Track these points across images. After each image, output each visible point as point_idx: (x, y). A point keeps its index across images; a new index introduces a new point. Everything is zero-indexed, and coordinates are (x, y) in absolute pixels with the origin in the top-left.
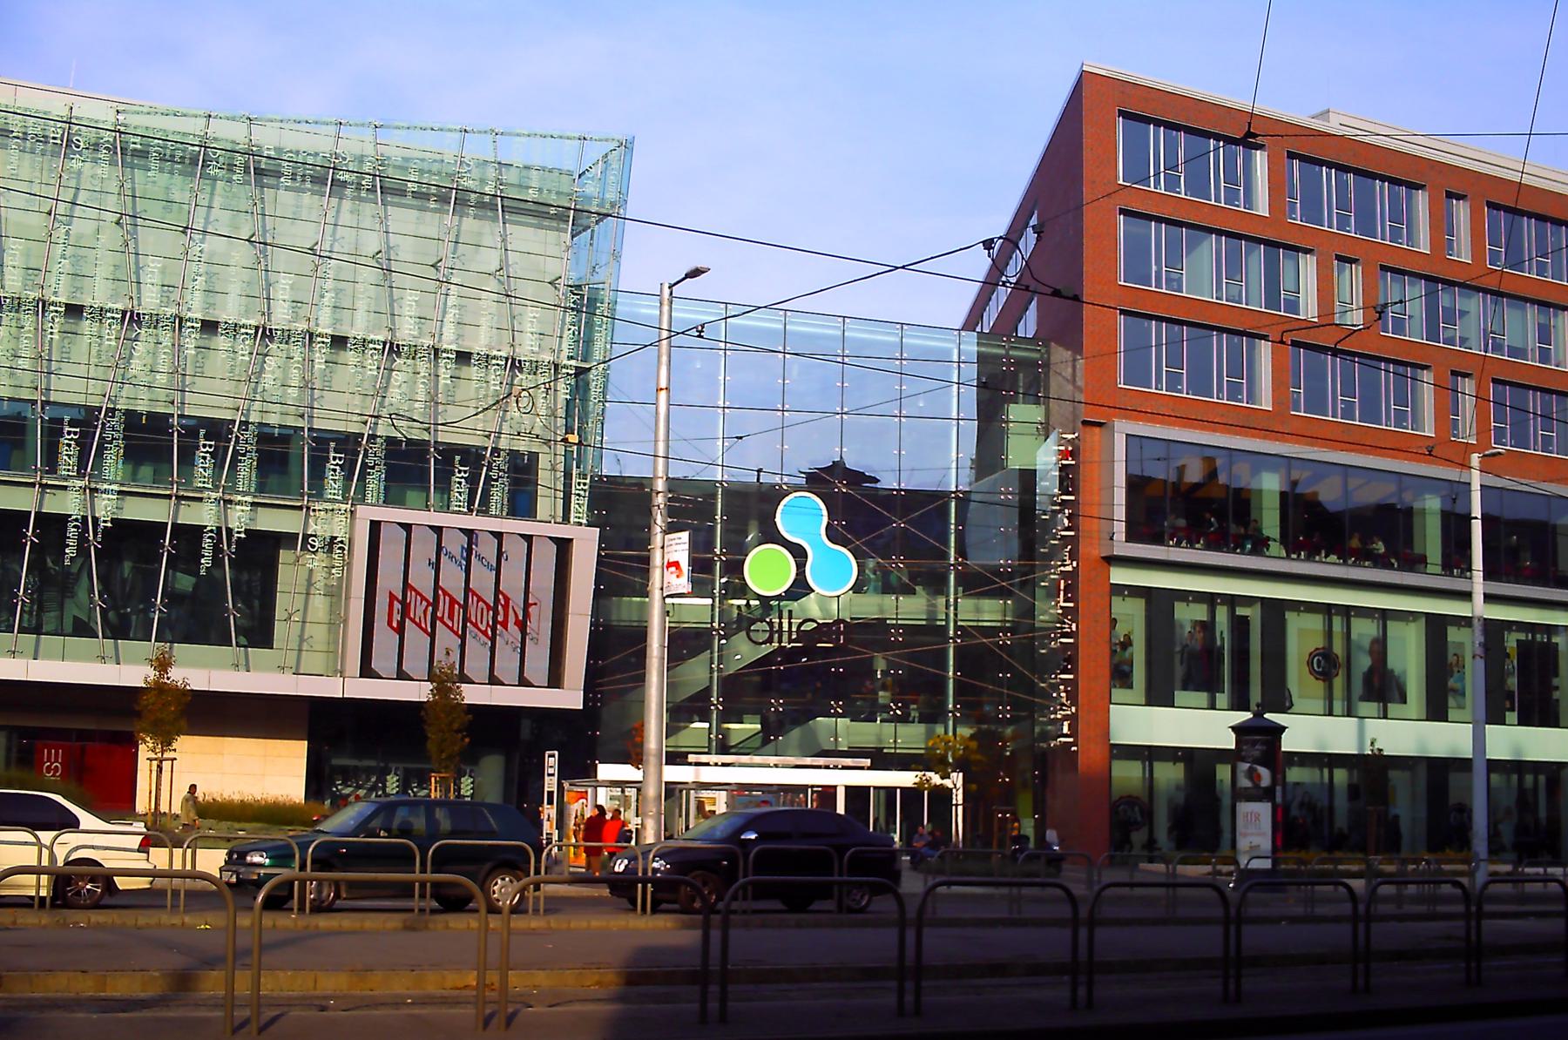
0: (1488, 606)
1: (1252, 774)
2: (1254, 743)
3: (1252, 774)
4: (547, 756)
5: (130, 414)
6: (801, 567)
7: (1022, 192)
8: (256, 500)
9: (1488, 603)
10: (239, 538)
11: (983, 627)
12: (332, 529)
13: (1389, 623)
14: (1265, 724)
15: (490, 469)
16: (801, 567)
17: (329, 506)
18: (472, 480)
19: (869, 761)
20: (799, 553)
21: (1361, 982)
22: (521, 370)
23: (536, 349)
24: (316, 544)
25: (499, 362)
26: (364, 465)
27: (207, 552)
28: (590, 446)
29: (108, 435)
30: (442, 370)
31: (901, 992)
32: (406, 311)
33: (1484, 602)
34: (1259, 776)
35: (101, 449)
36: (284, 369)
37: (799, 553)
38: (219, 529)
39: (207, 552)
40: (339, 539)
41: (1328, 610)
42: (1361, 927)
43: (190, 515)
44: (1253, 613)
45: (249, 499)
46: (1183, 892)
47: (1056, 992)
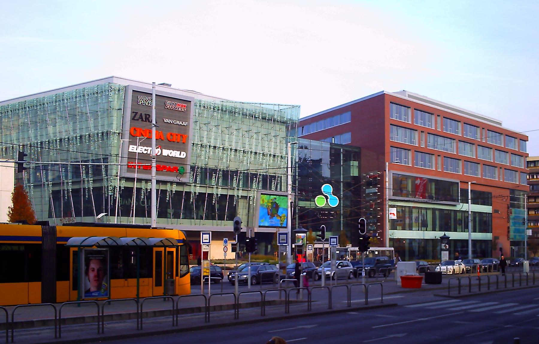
0: (126, 182)
1: (445, 246)
2: (446, 240)
3: (445, 246)
4: (201, 234)
7: (440, 100)
8: (201, 186)
9: (178, 186)
10: (123, 189)
11: (172, 206)
12: (115, 184)
13: (427, 210)
14: (446, 237)
19: (41, 242)
21: (58, 334)
24: (111, 188)
25: (117, 134)
28: (120, 157)
30: (232, 154)
33: (156, 184)
34: (446, 247)
37: (327, 198)
40: (116, 187)
41: (419, 208)
44: (407, 210)
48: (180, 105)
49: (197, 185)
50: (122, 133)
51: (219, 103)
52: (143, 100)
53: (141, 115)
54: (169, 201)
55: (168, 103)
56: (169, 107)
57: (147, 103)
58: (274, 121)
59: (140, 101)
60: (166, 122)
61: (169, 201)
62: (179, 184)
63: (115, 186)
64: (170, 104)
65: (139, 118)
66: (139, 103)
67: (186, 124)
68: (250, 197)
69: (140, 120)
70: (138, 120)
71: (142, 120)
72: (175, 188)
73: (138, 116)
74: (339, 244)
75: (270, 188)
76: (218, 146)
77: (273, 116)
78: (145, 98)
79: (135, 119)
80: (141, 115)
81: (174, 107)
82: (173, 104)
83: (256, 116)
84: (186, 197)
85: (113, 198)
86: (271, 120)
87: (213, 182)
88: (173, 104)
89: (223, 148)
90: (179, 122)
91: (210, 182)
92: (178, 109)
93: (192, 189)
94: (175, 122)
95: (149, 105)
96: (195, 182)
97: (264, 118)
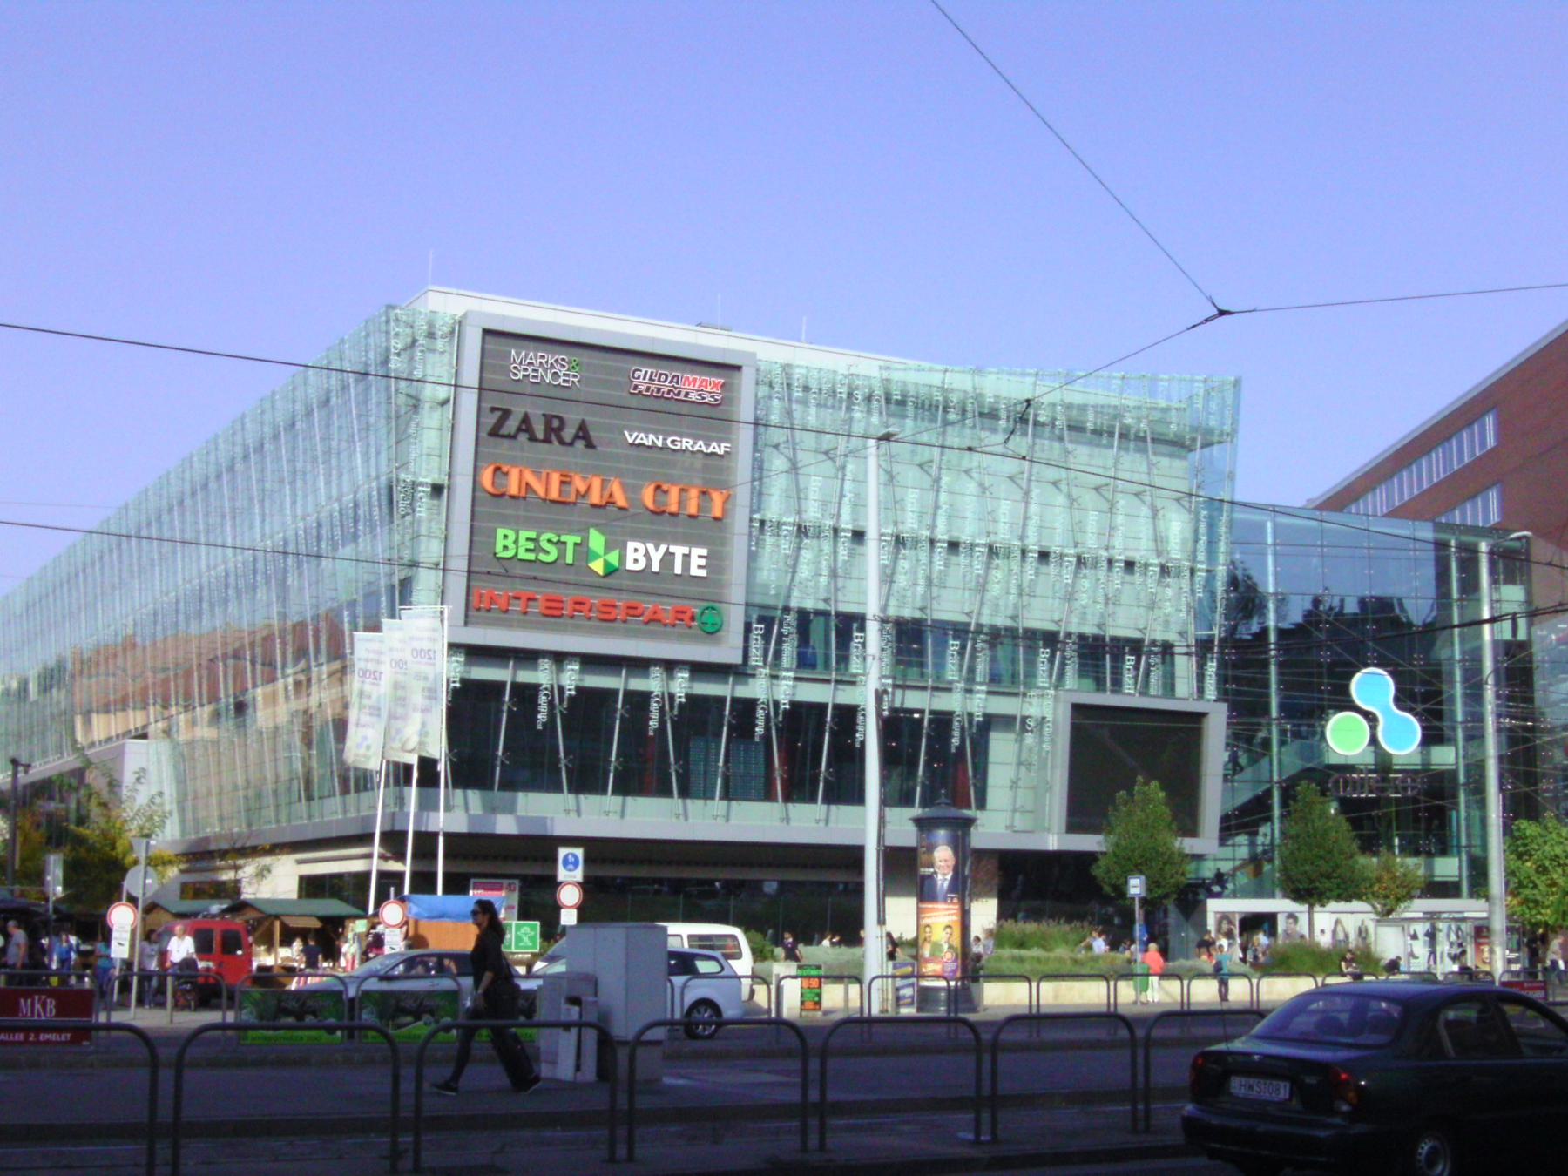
5: (1082, 637)
6: (1373, 728)
15: (781, 626)
16: (1373, 728)
17: (1040, 692)
18: (766, 637)
20: (1370, 717)
22: (904, 545)
23: (915, 526)
26: (780, 635)
27: (761, 722)
29: (785, 630)
31: (804, 1132)
32: (812, 496)
35: (779, 642)
36: (817, 562)
37: (1370, 717)
38: (552, 686)
39: (761, 722)
42: (1140, 1052)
43: (944, 702)
45: (791, 674)
46: (114, 1033)
47: (962, 1127)
48: (695, 380)
49: (784, 674)
50: (449, 488)
51: (875, 373)
52: (530, 364)
53: (526, 419)
54: (961, 748)
55: (642, 374)
56: (648, 389)
57: (550, 375)
58: (1124, 436)
59: (521, 368)
60: (632, 445)
61: (961, 748)
62: (700, 670)
63: (1044, 718)
64: (651, 379)
65: (519, 430)
66: (516, 375)
67: (723, 449)
68: (1024, 719)
69: (523, 437)
70: (513, 437)
71: (533, 438)
72: (681, 685)
73: (511, 425)
74: (782, 883)
75: (1117, 684)
76: (965, 537)
77: (1118, 414)
78: (543, 357)
79: (504, 431)
80: (526, 419)
81: (666, 390)
82: (663, 378)
83: (1042, 419)
84: (627, 711)
85: (1040, 756)
86: (1111, 434)
87: (952, 672)
88: (663, 378)
89: (1162, 567)
90: (691, 442)
91: (940, 666)
92: (687, 394)
93: (756, 689)
94: (673, 442)
95: (561, 380)
96: (970, 678)
97: (1076, 428)
